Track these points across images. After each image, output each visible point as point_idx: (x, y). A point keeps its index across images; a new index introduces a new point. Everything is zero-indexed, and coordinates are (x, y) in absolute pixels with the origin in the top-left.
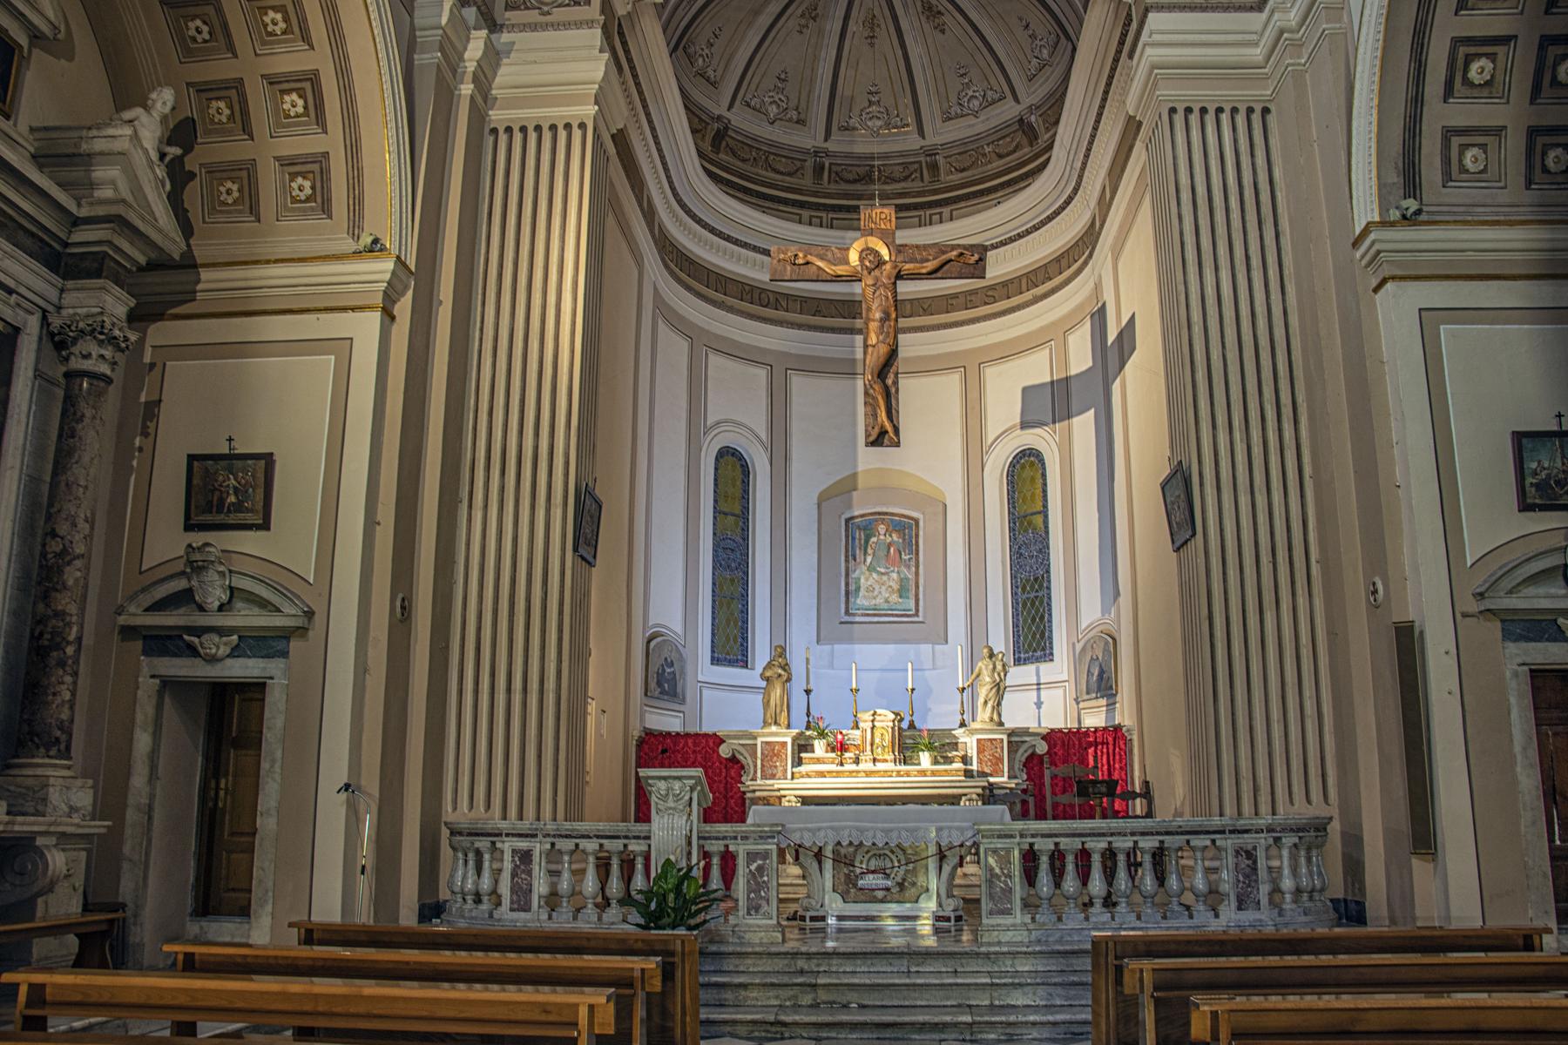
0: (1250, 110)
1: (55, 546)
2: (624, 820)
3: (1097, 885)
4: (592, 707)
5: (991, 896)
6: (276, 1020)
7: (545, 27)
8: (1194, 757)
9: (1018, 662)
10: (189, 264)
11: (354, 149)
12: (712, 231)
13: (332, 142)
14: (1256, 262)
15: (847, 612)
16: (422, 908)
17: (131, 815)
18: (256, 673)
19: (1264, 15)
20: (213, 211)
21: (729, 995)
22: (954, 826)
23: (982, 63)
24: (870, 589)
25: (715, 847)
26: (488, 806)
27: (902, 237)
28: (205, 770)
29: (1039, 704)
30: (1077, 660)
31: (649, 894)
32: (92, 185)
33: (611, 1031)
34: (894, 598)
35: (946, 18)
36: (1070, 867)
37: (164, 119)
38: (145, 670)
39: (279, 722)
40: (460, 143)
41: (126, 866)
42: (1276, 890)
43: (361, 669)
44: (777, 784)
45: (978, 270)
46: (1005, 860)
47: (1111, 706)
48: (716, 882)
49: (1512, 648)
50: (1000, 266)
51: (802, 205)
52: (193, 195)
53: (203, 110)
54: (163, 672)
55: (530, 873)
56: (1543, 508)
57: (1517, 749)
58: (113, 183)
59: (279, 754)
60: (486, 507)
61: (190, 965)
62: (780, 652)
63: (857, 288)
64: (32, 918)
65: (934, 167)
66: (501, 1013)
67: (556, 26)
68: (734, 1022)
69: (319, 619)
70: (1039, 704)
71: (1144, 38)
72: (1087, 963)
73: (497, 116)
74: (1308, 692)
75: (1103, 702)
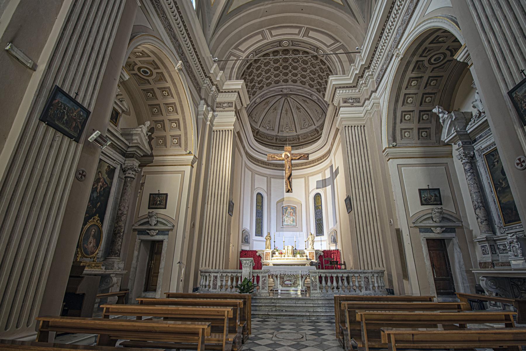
0: (361, 126)
1: (120, 212)
3: (335, 284)
4: (231, 245)
5: (313, 286)
6: (159, 316)
7: (224, 111)
8: (354, 256)
9: (317, 236)
10: (152, 156)
11: (186, 134)
12: (256, 151)
13: (182, 132)
16: (194, 289)
17: (132, 269)
20: (157, 145)
21: (258, 308)
24: (287, 221)
25: (255, 275)
26: (209, 266)
27: (293, 152)
29: (321, 245)
30: (329, 235)
31: (241, 285)
32: (132, 140)
33: (232, 317)
36: (329, 280)
37: (148, 127)
38: (138, 238)
39: (166, 249)
40: (207, 133)
41: (130, 281)
42: (374, 286)
43: (184, 237)
44: (268, 261)
45: (307, 158)
46: (315, 278)
47: (336, 245)
48: (255, 283)
49: (422, 234)
50: (311, 158)
51: (273, 146)
52: (153, 142)
53: (156, 125)
54: (142, 238)
56: (426, 205)
57: (425, 256)
58: (137, 139)
61: (142, 303)
62: (269, 233)
63: (284, 162)
64: (108, 292)
65: (299, 139)
66: (208, 313)
68: (259, 314)
69: (175, 227)
70: (321, 245)
71: (340, 112)
72: (333, 302)
73: (214, 128)
74: (378, 243)
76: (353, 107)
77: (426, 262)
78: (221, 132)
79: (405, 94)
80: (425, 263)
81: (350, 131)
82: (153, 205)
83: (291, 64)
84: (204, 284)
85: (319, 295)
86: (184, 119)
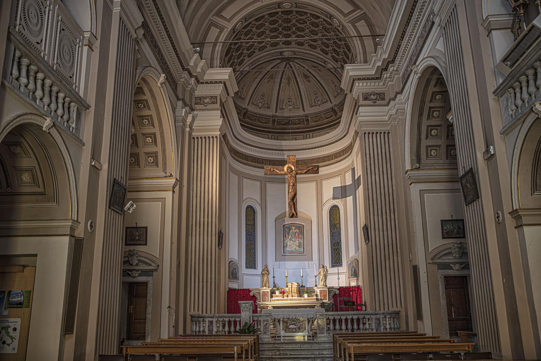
0: (385, 133)
2: (225, 313)
7: (206, 110)
11: (164, 151)
12: (244, 143)
13: (159, 149)
14: (385, 173)
15: (284, 252)
18: (145, 280)
19: (389, 107)
22: (311, 313)
23: (321, 92)
24: (290, 246)
26: (198, 311)
28: (128, 303)
29: (339, 279)
30: (349, 266)
34: (297, 248)
35: (311, 79)
36: (337, 323)
39: (151, 292)
44: (267, 303)
47: (357, 279)
49: (440, 271)
51: (269, 132)
55: (212, 326)
57: (441, 295)
59: (151, 299)
60: (196, 236)
65: (307, 120)
67: (208, 110)
70: (339, 279)
73: (194, 134)
75: (356, 278)
76: (376, 106)
77: (442, 302)
78: (204, 140)
79: (430, 108)
80: (441, 303)
81: (371, 139)
82: (131, 240)
83: (294, 25)
84: (197, 330)
85: (326, 339)
86: (162, 133)
